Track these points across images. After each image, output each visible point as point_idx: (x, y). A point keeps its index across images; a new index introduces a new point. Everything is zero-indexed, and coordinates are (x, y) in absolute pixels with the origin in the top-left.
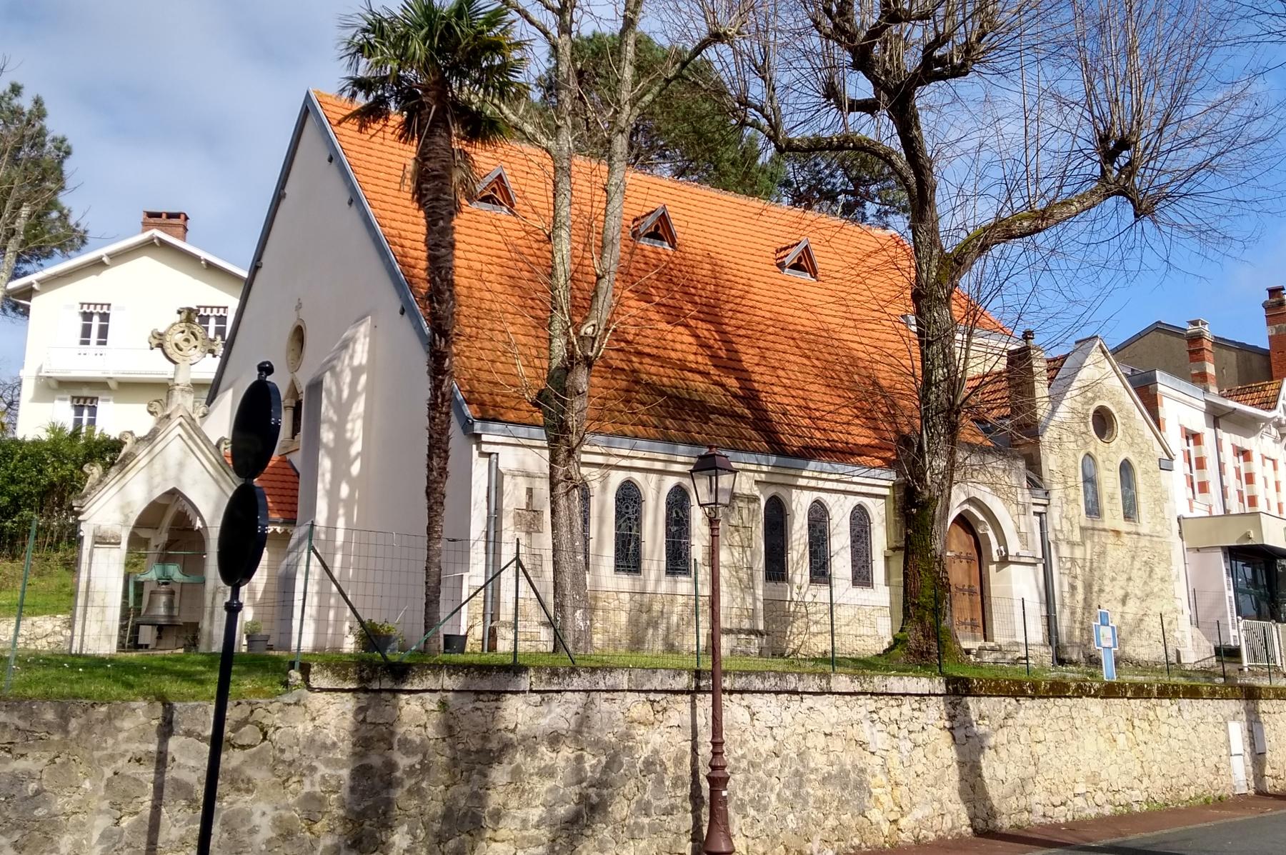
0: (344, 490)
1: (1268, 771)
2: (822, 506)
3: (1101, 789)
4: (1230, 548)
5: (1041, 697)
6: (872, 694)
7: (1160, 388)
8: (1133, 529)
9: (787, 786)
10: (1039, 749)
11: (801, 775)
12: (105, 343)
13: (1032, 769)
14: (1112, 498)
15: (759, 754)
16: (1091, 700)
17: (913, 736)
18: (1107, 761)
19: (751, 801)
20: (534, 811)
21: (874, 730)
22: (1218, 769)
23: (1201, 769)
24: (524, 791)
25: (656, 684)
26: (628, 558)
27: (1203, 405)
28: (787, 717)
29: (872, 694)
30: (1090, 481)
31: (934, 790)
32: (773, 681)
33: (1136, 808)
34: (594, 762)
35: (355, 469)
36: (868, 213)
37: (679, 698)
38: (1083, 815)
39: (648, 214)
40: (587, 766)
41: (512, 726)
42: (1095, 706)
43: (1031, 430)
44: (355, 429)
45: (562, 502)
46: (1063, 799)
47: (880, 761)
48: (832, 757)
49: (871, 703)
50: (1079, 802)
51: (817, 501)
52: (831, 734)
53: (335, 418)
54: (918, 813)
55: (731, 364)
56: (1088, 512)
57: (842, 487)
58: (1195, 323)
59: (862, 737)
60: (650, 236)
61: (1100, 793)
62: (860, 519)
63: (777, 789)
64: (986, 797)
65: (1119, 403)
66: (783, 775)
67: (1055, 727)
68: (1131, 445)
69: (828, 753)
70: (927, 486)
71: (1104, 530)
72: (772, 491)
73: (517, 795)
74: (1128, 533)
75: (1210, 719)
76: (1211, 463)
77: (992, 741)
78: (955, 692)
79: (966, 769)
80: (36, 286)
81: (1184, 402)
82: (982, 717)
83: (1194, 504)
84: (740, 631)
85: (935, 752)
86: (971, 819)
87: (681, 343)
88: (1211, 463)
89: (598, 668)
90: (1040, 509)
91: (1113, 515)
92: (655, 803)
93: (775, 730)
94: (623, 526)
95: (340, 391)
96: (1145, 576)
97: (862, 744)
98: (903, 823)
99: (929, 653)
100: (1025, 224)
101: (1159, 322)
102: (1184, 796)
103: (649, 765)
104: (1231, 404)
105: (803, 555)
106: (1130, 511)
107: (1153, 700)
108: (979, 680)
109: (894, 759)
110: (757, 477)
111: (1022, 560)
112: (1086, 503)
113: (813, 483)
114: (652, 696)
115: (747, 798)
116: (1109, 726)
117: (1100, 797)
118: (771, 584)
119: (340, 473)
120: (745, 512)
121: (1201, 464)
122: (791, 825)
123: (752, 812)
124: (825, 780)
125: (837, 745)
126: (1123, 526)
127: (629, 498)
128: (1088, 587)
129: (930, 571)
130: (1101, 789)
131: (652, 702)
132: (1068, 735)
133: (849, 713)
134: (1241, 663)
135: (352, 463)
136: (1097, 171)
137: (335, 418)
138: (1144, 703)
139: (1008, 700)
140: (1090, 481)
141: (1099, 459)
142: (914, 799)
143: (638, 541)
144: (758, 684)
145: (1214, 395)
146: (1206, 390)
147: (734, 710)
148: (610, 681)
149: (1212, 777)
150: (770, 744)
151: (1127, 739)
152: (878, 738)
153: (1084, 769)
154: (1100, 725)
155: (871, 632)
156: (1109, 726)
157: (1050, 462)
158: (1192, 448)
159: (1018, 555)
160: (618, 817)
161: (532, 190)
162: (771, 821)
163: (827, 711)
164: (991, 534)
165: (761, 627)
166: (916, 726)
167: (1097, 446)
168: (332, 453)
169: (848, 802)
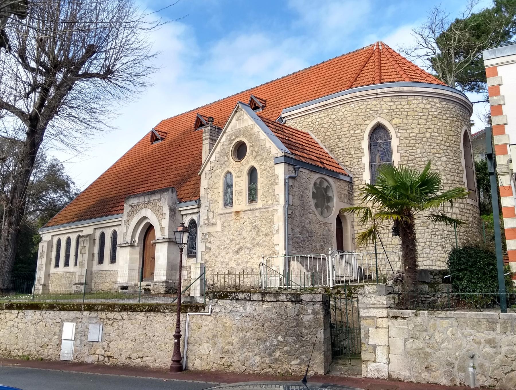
74: (245, 211)
90: (196, 210)
91: (240, 201)
106: (252, 196)
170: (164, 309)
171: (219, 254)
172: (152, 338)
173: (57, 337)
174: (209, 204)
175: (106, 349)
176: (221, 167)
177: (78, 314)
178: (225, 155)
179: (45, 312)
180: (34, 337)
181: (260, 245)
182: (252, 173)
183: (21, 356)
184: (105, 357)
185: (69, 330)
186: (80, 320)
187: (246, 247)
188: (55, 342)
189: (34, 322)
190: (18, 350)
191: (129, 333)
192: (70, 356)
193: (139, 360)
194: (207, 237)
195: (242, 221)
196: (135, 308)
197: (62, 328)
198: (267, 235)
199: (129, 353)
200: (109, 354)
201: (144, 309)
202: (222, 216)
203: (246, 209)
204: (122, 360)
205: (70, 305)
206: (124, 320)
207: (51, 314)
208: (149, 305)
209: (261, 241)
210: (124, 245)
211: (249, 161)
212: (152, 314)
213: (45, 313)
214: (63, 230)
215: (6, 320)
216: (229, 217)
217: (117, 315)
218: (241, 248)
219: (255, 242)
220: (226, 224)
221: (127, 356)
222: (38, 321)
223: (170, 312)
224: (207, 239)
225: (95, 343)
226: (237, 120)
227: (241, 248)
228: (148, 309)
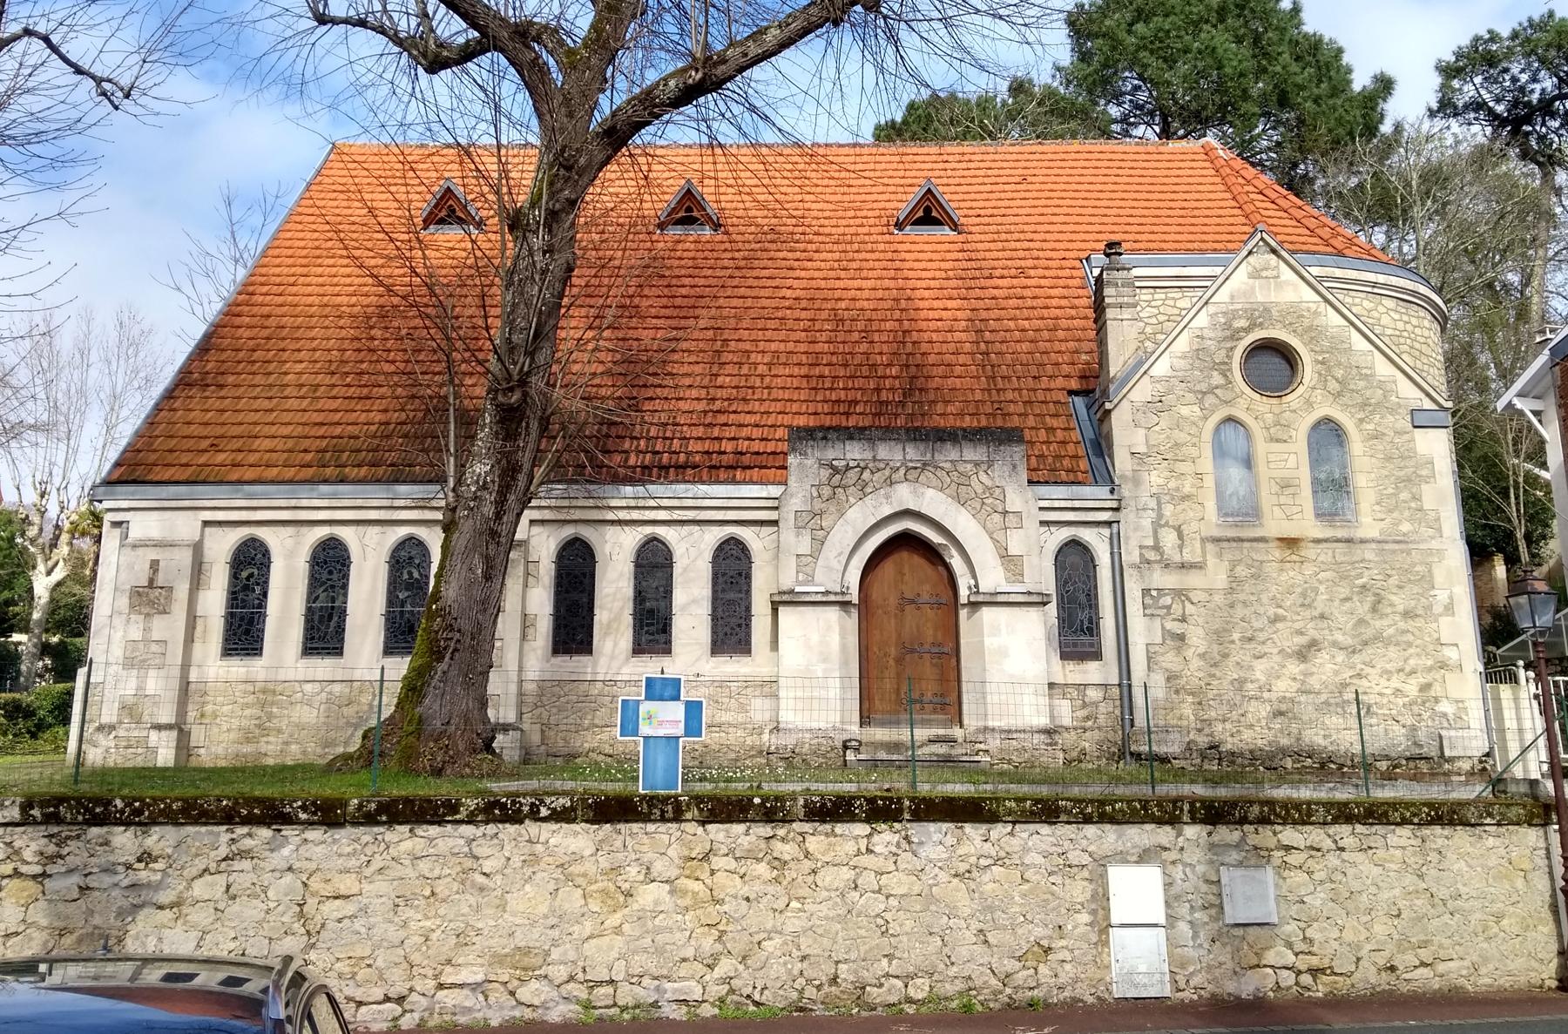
8: (1340, 534)
42: (577, 839)
46: (399, 989)
57: (691, 515)
74: (1318, 541)
90: (1105, 516)
94: (323, 596)
96: (1362, 608)
111: (1000, 598)
113: (635, 515)
128: (1220, 636)
155: (740, 718)
161: (1204, 172)
167: (1250, 404)
170: (1481, 816)
171: (1225, 656)
172: (1450, 903)
173: (1085, 918)
174: (1159, 503)
175: (1300, 946)
176: (1201, 401)
177: (1164, 834)
178: (1213, 369)
179: (1009, 827)
180: (975, 925)
181: (1388, 642)
182: (1328, 434)
183: (923, 1002)
184: (1299, 973)
185: (1137, 891)
186: (1173, 855)
187: (1334, 644)
188: (1083, 938)
189: (963, 867)
190: (907, 979)
191: (1373, 890)
192: (1162, 982)
193: (1422, 971)
194: (1167, 600)
195: (1309, 570)
196: (1385, 814)
197: (1105, 887)
198: (1408, 614)
199: (1386, 954)
200: (1315, 961)
201: (1415, 815)
202: (1225, 544)
203: (1320, 536)
204: (1368, 977)
205: (1129, 802)
206: (1342, 849)
207: (1037, 840)
208: (1430, 805)
209: (1391, 631)
210: (819, 598)
211: (1309, 400)
212: (1438, 829)
213: (1011, 834)
214: (272, 503)
215: (807, 865)
216: (1257, 551)
217: (1315, 835)
218: (1314, 644)
219: (1368, 633)
220: (1241, 571)
221: (1381, 962)
222: (983, 862)
223: (1499, 824)
224: (1169, 607)
225: (1251, 930)
226: (1251, 276)
227: (1314, 644)
228: (1428, 815)
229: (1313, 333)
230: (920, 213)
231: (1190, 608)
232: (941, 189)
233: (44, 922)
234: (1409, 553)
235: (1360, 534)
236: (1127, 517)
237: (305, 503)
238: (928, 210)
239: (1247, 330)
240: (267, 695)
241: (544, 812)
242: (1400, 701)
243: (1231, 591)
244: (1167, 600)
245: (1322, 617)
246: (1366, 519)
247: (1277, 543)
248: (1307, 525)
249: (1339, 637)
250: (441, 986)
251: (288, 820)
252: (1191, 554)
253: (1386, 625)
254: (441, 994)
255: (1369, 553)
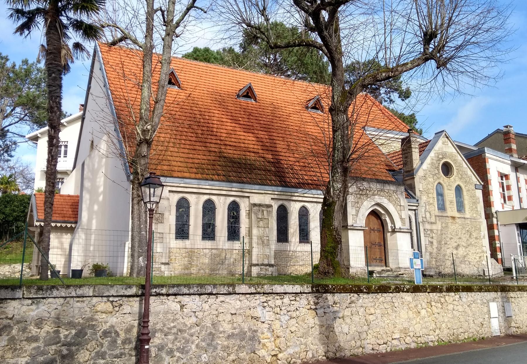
0: (96, 207)
1: (513, 324)
2: (306, 208)
3: (409, 336)
4: (519, 224)
5: (373, 293)
6: (264, 293)
7: (487, 155)
8: (462, 216)
9: (203, 340)
10: (371, 318)
11: (214, 335)
12: (66, 157)
13: (366, 328)
14: (451, 202)
15: (185, 325)
16: (405, 294)
17: (290, 313)
18: (414, 322)
19: (177, 349)
20: (22, 359)
21: (264, 311)
22: (483, 325)
23: (472, 325)
24: (15, 350)
25: (113, 292)
26: (182, 232)
27: (510, 162)
28: (206, 306)
29: (264, 293)
30: (440, 195)
31: (302, 339)
32: (196, 289)
33: (431, 344)
34: (67, 333)
35: (101, 198)
36: (381, 92)
37: (131, 299)
38: (397, 348)
39: (310, 100)
40: (62, 336)
41: (10, 316)
42: (408, 297)
43: (410, 174)
44: (101, 180)
45: (136, 207)
46: (385, 341)
47: (267, 326)
48: (235, 325)
49: (263, 298)
50: (395, 342)
51: (303, 207)
52: (235, 314)
53: (91, 177)
54: (291, 351)
55: (271, 149)
56: (439, 209)
58: (506, 127)
59: (256, 315)
60: (244, 96)
61: (408, 338)
62: (304, 214)
63: (197, 342)
64: (336, 341)
65: (455, 160)
66: (201, 335)
67: (382, 307)
68: (461, 179)
69: (233, 324)
70: (331, 196)
71: (447, 217)
72: (280, 202)
73: (11, 351)
74: (459, 218)
75: (479, 301)
76: (514, 188)
77: (341, 315)
78: (318, 291)
79: (324, 329)
80: (39, 135)
81: (500, 161)
82: (335, 303)
83: (505, 205)
84: (263, 265)
85: (303, 320)
86: (325, 353)
87: (249, 140)
88: (514, 188)
89: (71, 286)
90: (414, 208)
91: (452, 210)
92: (109, 352)
93: (197, 313)
95: (94, 165)
96: (468, 236)
97: (257, 318)
98: (280, 356)
99: (329, 273)
100: (384, 74)
101: (499, 129)
102: (461, 337)
103: (106, 334)
104: (522, 161)
105: (296, 231)
106: (460, 207)
107: (444, 294)
108: (332, 285)
109: (277, 325)
110: (273, 196)
111: (402, 230)
112: (438, 205)
113: (300, 199)
114: (111, 299)
115: (175, 347)
116: (416, 306)
117: (408, 340)
118: (280, 244)
119: (92, 202)
120: (265, 212)
121: (509, 188)
122: (204, 360)
123: (178, 354)
124: (229, 337)
125: (239, 319)
126: (457, 215)
127: (183, 207)
128: (439, 242)
129: (331, 235)
130: (409, 336)
131: (112, 302)
132: (390, 311)
133: (248, 303)
134: (512, 274)
135: (99, 196)
136: (422, 50)
137: (91, 177)
138: (438, 294)
139: (352, 295)
140: (440, 195)
141: (445, 185)
142: (288, 344)
143: (214, 226)
144: (185, 291)
145: (515, 158)
146: (512, 156)
147: (155, 304)
148: (80, 292)
149: (478, 329)
150: (194, 320)
151: (427, 312)
152: (267, 315)
153: (399, 326)
154: (410, 306)
156: (416, 306)
157: (419, 185)
158: (504, 181)
159: (400, 229)
160: (81, 360)
162: (191, 358)
163: (233, 303)
164: (388, 219)
165: (273, 262)
166: (292, 308)
167: (443, 179)
168: (90, 192)
169: (244, 347)
181: (473, 245)
182: (458, 189)
187: (463, 245)
210: (360, 228)
229: (455, 161)
230: (245, 94)
231: (434, 235)
232: (177, 73)
233: (318, 323)
234: (476, 222)
235: (466, 216)
236: (419, 208)
237: (204, 187)
238: (248, 93)
239: (442, 158)
240: (191, 253)
241: (405, 290)
242: (476, 261)
243: (441, 230)
244: (429, 232)
245: (460, 238)
246: (467, 212)
247: (450, 218)
248: (457, 215)
249: (464, 244)
250: (392, 339)
251: (362, 292)
252: (433, 220)
253: (473, 241)
254: (393, 341)
255: (468, 221)
